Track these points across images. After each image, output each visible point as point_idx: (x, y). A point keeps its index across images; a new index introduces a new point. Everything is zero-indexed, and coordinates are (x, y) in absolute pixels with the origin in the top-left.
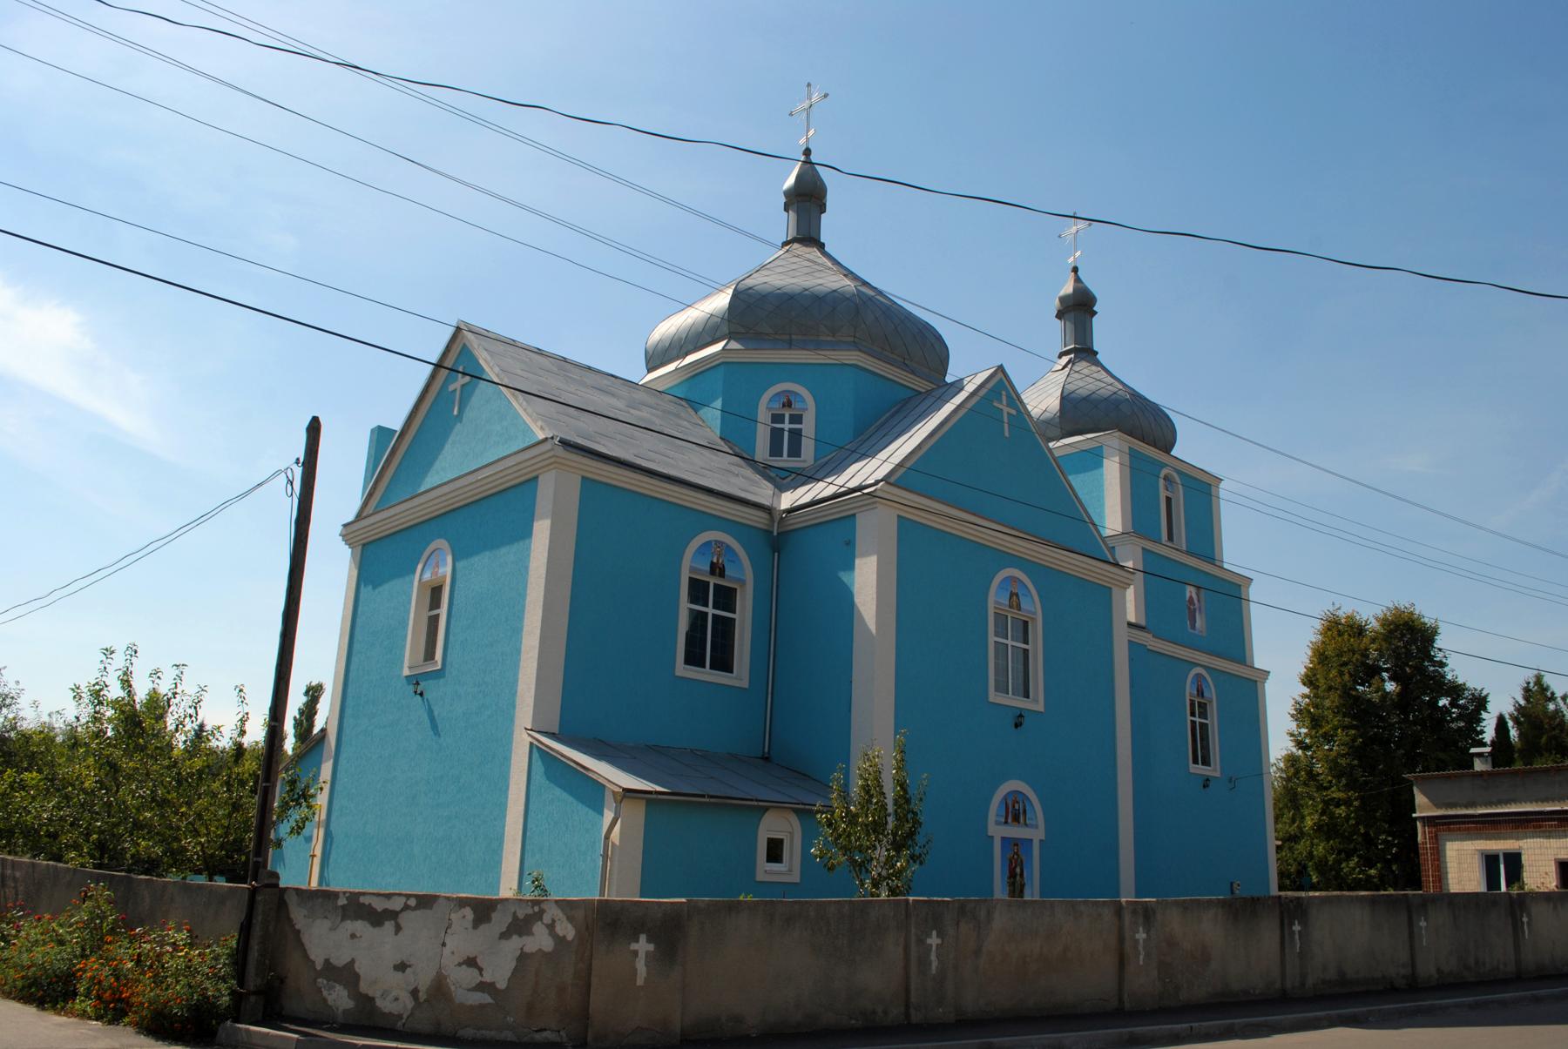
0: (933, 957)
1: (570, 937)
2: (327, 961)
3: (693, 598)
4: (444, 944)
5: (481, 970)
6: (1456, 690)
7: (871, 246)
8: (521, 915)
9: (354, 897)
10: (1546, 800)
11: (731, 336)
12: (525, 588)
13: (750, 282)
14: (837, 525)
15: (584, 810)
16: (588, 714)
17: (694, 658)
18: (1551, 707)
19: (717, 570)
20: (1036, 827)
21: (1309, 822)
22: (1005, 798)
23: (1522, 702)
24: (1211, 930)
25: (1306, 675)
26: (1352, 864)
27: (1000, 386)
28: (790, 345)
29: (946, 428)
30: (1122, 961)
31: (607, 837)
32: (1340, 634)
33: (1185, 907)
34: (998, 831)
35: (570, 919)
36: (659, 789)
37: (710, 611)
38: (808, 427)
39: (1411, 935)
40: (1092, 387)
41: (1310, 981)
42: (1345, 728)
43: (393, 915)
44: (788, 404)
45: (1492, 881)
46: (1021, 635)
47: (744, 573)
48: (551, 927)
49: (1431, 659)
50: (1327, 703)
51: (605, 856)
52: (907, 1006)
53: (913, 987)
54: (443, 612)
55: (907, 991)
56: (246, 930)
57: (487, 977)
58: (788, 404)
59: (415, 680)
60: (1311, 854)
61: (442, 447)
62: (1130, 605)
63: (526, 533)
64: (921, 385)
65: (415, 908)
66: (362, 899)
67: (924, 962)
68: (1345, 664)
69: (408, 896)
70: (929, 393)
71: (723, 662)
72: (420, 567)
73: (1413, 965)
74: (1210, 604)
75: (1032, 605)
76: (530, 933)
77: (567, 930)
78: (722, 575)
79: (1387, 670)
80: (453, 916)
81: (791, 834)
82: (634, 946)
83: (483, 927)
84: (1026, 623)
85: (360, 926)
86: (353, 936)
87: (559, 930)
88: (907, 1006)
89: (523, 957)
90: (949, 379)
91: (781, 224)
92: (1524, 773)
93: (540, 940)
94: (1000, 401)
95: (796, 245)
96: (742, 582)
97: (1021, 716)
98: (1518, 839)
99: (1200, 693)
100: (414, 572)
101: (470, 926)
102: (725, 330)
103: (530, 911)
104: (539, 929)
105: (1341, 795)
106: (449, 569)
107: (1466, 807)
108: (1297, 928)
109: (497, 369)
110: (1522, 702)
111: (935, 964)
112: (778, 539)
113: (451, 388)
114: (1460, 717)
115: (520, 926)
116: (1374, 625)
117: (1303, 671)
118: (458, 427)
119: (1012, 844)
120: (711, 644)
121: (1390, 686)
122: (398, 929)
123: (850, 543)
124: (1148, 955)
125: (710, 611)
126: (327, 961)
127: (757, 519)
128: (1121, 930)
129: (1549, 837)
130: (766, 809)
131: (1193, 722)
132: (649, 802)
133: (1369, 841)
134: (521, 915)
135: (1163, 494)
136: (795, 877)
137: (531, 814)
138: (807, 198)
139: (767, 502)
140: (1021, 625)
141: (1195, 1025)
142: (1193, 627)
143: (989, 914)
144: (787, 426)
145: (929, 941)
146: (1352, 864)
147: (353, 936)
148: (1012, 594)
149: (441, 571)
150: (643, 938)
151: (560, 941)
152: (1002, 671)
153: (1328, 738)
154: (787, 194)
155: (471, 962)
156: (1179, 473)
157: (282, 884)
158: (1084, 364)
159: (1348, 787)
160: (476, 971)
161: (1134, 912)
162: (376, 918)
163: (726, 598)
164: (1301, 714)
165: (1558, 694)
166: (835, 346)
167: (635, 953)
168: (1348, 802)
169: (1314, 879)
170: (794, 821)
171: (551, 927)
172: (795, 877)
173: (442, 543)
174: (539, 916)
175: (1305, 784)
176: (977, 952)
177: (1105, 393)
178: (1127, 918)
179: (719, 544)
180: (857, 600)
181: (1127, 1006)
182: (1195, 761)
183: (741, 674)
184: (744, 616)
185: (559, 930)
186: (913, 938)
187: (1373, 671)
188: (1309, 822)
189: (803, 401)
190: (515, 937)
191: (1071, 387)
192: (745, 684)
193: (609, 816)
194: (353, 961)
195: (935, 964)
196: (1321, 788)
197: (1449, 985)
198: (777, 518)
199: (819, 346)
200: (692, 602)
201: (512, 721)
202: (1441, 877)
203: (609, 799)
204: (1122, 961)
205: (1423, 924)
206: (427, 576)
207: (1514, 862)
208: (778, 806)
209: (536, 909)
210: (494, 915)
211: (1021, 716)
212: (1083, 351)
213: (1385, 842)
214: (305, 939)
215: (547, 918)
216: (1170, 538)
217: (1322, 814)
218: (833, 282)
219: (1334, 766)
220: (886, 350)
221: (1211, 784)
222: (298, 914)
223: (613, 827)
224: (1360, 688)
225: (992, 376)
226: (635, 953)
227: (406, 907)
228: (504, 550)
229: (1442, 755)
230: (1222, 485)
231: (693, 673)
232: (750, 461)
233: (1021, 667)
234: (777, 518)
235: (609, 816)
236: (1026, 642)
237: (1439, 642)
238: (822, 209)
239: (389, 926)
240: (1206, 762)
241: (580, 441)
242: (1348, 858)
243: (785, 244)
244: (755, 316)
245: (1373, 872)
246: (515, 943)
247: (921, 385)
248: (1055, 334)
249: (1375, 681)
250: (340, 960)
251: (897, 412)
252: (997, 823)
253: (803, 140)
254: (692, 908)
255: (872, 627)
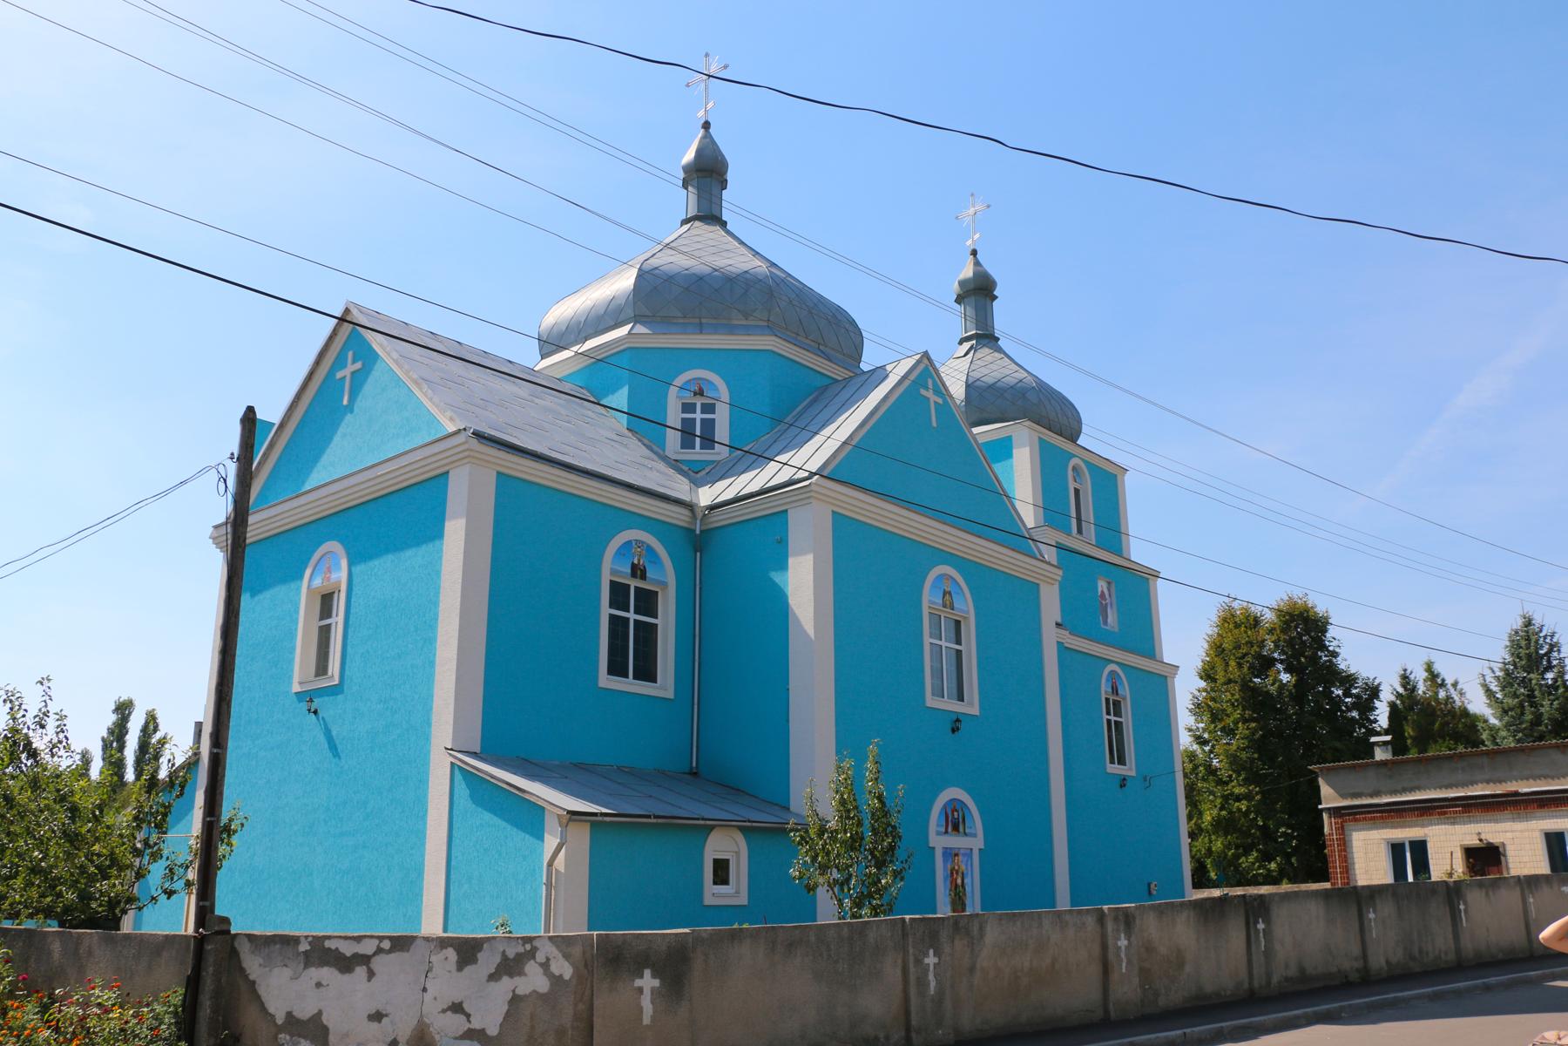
0: (931, 977)
1: (567, 976)
2: (289, 1014)
3: (614, 603)
4: (425, 990)
5: (468, 1016)
6: (1348, 680)
7: (781, 226)
8: (511, 954)
9: (317, 941)
10: (1449, 786)
11: (637, 319)
12: (437, 594)
13: (654, 262)
14: (766, 523)
15: (518, 838)
16: (516, 734)
17: (616, 668)
18: (1442, 694)
19: (638, 571)
20: (975, 835)
21: (1207, 817)
22: (945, 806)
23: (1401, 690)
24: (1184, 933)
25: (1204, 670)
26: (1251, 859)
27: (926, 371)
28: (701, 328)
29: (872, 422)
30: (1106, 969)
31: (550, 864)
32: (1237, 626)
33: (1161, 910)
34: (939, 841)
35: (567, 957)
36: (605, 810)
37: (632, 616)
38: (722, 417)
39: (1362, 930)
40: (997, 375)
41: (1275, 980)
42: (1245, 721)
43: (364, 960)
44: (700, 393)
45: (1399, 871)
46: (953, 635)
47: (666, 577)
48: (545, 966)
49: (1324, 647)
50: (1226, 696)
51: (549, 885)
52: (908, 1029)
53: (913, 1009)
54: (337, 620)
55: (907, 1013)
56: (193, 985)
57: (476, 1024)
58: (700, 393)
59: (308, 697)
60: (1209, 850)
61: (331, 439)
62: (1051, 606)
63: (437, 534)
64: (838, 373)
65: (390, 951)
66: (327, 944)
67: (922, 983)
68: (1245, 655)
69: (381, 938)
70: (847, 380)
71: (647, 672)
72: (308, 572)
73: (1365, 956)
74: (1116, 594)
75: (965, 605)
76: (521, 973)
77: (564, 969)
78: (643, 577)
79: (1282, 662)
80: (433, 958)
81: (737, 853)
82: (638, 983)
83: (469, 969)
84: (958, 623)
85: (327, 974)
86: (319, 985)
87: (555, 968)
88: (908, 1029)
89: (515, 1000)
90: (865, 367)
91: (682, 201)
92: (1419, 760)
93: (533, 981)
94: (927, 389)
95: (697, 223)
96: (664, 585)
97: (958, 720)
98: (1423, 826)
99: (1115, 690)
100: (301, 577)
101: (453, 967)
102: (630, 312)
103: (521, 950)
104: (532, 968)
105: (1243, 790)
106: (343, 575)
107: (1371, 796)
108: (1261, 926)
109: (395, 355)
110: (1401, 690)
111: (933, 984)
112: (700, 539)
113: (339, 375)
114: (1354, 706)
115: (510, 967)
116: (1269, 616)
117: (1200, 665)
118: (349, 417)
119: (951, 854)
120: (633, 652)
121: (1285, 677)
122: (371, 974)
123: (782, 542)
124: (1129, 962)
125: (632, 616)
126: (289, 1014)
127: (679, 516)
128: (1104, 936)
129: (1453, 824)
130: (712, 828)
131: (1109, 721)
132: (593, 824)
133: (1268, 835)
134: (511, 954)
135: (1072, 486)
136: (743, 900)
137: (456, 841)
138: (708, 173)
139: (686, 497)
140: (953, 624)
141: (1188, 1031)
142: (1106, 623)
143: (981, 929)
144: (698, 416)
145: (927, 961)
146: (1251, 859)
147: (319, 985)
148: (945, 593)
149: (334, 576)
150: (647, 973)
151: (556, 980)
152: (938, 673)
153: (1229, 732)
154: (686, 169)
155: (457, 1008)
156: (1087, 463)
157: (233, 932)
158: (986, 351)
159: (1247, 782)
160: (463, 1018)
161: (1116, 919)
162: (345, 964)
163: (647, 601)
164: (1198, 708)
165: (1449, 681)
166: (748, 330)
167: (640, 990)
168: (1248, 797)
169: (1213, 875)
170: (740, 838)
171: (545, 966)
172: (743, 900)
173: (334, 546)
174: (532, 954)
175: (1203, 779)
176: (972, 969)
177: (1011, 381)
178: (1110, 926)
179: (640, 543)
180: (792, 602)
181: (1113, 1015)
182: (1112, 762)
183: (665, 684)
184: (666, 621)
185: (555, 968)
186: (911, 959)
187: (1268, 663)
188: (1207, 817)
189: (717, 390)
190: (505, 979)
191: (976, 375)
192: (670, 694)
193: (551, 842)
194: (320, 1013)
195: (933, 984)
196: (1220, 782)
197: (1400, 976)
198: (700, 515)
199: (731, 330)
200: (611, 606)
201: (428, 738)
202: (1347, 869)
203: (552, 824)
204: (1106, 969)
205: (1372, 916)
206: (317, 582)
207: (1420, 848)
208: (725, 824)
209: (528, 947)
210: (479, 955)
211: (958, 720)
212: (985, 337)
213: (1284, 834)
214: (262, 991)
215: (540, 957)
216: (1080, 531)
217: (1222, 808)
218: (739, 262)
219: (1233, 760)
220: (803, 341)
221: (1128, 784)
222: (252, 964)
223: (557, 853)
224: (1257, 680)
225: (919, 362)
226: (640, 990)
227: (379, 951)
228: (409, 553)
229: (1338, 744)
230: (1127, 477)
231: (617, 683)
232: (665, 459)
233: (954, 668)
234: (700, 515)
235: (551, 842)
236: (958, 642)
237: (1332, 632)
238: (723, 184)
239: (360, 971)
240: (1122, 761)
241: (493, 433)
242: (1247, 853)
243: (685, 222)
244: (664, 298)
245: (1273, 866)
246: (506, 984)
247: (838, 373)
248: (956, 321)
249: (1271, 672)
250: (304, 1012)
251: (815, 400)
252: (938, 833)
253: (701, 113)
254: (697, 939)
255: (811, 631)
